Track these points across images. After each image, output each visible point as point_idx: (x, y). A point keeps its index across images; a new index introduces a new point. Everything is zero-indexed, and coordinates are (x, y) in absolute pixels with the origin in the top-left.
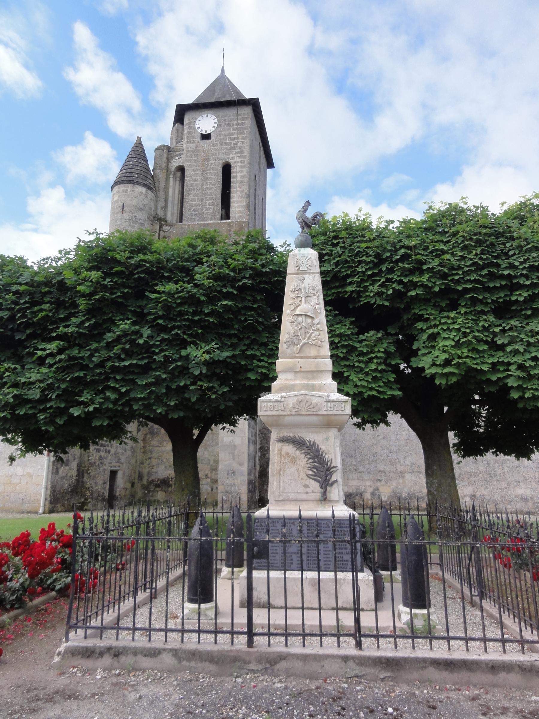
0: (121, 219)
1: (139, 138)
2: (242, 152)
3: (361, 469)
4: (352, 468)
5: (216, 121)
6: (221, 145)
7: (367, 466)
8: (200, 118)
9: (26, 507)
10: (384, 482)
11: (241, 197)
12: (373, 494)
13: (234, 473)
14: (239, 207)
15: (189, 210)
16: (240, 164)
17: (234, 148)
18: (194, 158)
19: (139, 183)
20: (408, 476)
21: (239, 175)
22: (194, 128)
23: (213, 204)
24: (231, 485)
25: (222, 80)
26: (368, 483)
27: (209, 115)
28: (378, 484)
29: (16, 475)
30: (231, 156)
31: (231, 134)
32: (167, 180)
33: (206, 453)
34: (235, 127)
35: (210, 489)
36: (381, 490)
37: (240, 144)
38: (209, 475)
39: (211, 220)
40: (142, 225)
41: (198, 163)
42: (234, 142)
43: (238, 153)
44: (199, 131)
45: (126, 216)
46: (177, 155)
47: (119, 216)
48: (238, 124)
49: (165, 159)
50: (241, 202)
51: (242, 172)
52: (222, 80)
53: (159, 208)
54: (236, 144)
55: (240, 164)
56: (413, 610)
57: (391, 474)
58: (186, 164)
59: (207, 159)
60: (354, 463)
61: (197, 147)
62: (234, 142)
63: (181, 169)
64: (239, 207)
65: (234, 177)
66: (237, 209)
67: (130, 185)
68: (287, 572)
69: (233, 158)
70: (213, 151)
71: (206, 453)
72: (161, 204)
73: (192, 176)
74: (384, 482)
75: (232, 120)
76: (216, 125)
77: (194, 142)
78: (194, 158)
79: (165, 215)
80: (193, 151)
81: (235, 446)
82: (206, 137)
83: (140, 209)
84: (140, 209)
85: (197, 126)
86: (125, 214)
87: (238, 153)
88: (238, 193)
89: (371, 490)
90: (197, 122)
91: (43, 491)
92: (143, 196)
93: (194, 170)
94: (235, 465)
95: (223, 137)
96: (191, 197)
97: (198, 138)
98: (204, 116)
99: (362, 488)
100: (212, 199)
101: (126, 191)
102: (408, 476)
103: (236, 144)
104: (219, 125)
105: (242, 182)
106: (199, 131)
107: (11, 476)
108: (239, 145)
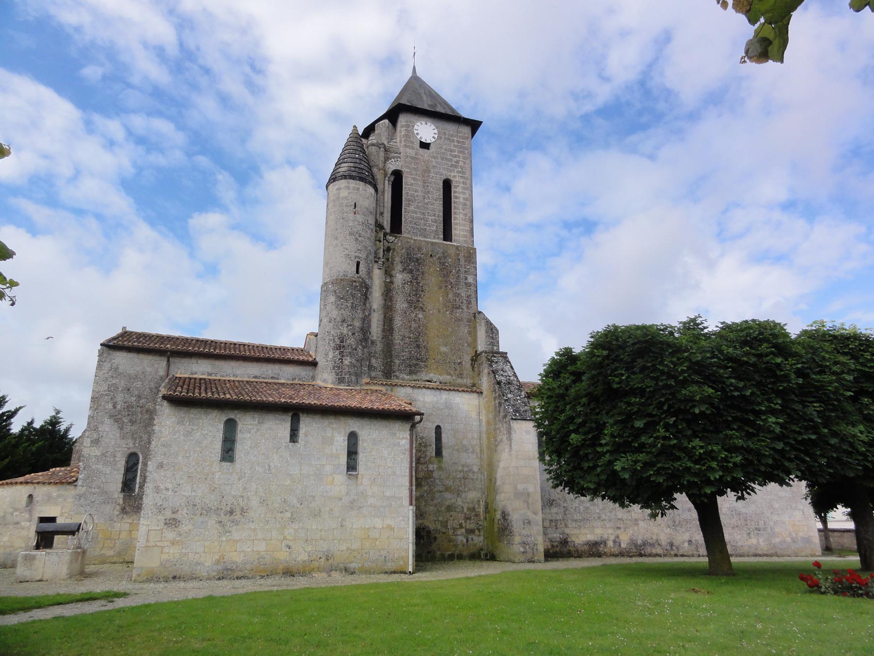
0: (354, 220)
2: (463, 173)
3: (603, 517)
4: (596, 516)
5: (436, 131)
6: (442, 159)
7: (608, 514)
8: (419, 124)
9: (390, 566)
10: (622, 530)
11: (465, 220)
12: (614, 542)
13: (529, 523)
14: (463, 231)
16: (461, 185)
17: (456, 167)
18: (413, 165)
20: (641, 523)
21: (461, 196)
22: (413, 133)
24: (527, 536)
25: (415, 83)
26: (610, 531)
27: (429, 124)
28: (618, 532)
29: (374, 528)
30: (453, 174)
31: (452, 151)
33: (459, 500)
34: (456, 143)
35: (465, 540)
36: (621, 537)
37: (461, 164)
38: (464, 525)
39: (434, 238)
41: (419, 173)
42: (455, 159)
43: (460, 172)
44: (419, 137)
45: (359, 217)
46: (394, 157)
47: (351, 216)
48: (459, 142)
49: (382, 159)
50: (464, 225)
51: (464, 193)
52: (415, 83)
54: (457, 162)
57: (628, 522)
59: (427, 171)
60: (597, 511)
61: (416, 154)
62: (455, 159)
64: (463, 231)
65: (456, 198)
67: (362, 183)
69: (454, 176)
70: (434, 164)
71: (459, 500)
74: (622, 530)
75: (452, 136)
76: (436, 136)
77: (413, 148)
78: (413, 165)
80: (413, 158)
81: (528, 494)
82: (425, 146)
85: (416, 132)
87: (460, 172)
88: (462, 216)
89: (612, 538)
90: (416, 127)
91: (411, 546)
93: (414, 179)
94: (530, 515)
95: (443, 151)
96: (412, 208)
97: (418, 145)
98: (423, 123)
99: (605, 536)
101: (358, 189)
102: (641, 523)
103: (457, 162)
104: (439, 137)
105: (465, 204)
106: (419, 137)
107: (369, 529)
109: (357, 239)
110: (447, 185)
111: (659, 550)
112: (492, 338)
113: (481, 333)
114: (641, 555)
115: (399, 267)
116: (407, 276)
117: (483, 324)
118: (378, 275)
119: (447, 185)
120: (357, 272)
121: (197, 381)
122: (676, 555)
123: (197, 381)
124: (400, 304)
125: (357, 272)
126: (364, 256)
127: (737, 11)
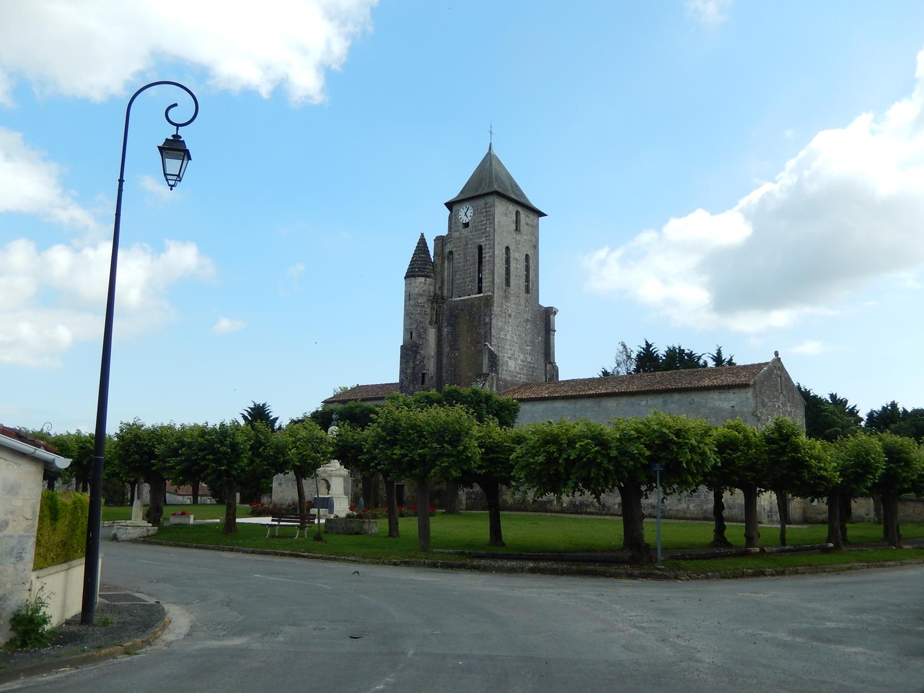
1: (422, 235)
17: (484, 233)
19: (419, 276)
32: (443, 263)
40: (423, 306)
63: (451, 253)
82: (466, 225)
83: (421, 295)
84: (421, 295)
93: (459, 254)
97: (461, 227)
104: (474, 214)
110: (480, 248)
114: (577, 513)
118: (432, 333)
122: (606, 514)
124: (446, 349)
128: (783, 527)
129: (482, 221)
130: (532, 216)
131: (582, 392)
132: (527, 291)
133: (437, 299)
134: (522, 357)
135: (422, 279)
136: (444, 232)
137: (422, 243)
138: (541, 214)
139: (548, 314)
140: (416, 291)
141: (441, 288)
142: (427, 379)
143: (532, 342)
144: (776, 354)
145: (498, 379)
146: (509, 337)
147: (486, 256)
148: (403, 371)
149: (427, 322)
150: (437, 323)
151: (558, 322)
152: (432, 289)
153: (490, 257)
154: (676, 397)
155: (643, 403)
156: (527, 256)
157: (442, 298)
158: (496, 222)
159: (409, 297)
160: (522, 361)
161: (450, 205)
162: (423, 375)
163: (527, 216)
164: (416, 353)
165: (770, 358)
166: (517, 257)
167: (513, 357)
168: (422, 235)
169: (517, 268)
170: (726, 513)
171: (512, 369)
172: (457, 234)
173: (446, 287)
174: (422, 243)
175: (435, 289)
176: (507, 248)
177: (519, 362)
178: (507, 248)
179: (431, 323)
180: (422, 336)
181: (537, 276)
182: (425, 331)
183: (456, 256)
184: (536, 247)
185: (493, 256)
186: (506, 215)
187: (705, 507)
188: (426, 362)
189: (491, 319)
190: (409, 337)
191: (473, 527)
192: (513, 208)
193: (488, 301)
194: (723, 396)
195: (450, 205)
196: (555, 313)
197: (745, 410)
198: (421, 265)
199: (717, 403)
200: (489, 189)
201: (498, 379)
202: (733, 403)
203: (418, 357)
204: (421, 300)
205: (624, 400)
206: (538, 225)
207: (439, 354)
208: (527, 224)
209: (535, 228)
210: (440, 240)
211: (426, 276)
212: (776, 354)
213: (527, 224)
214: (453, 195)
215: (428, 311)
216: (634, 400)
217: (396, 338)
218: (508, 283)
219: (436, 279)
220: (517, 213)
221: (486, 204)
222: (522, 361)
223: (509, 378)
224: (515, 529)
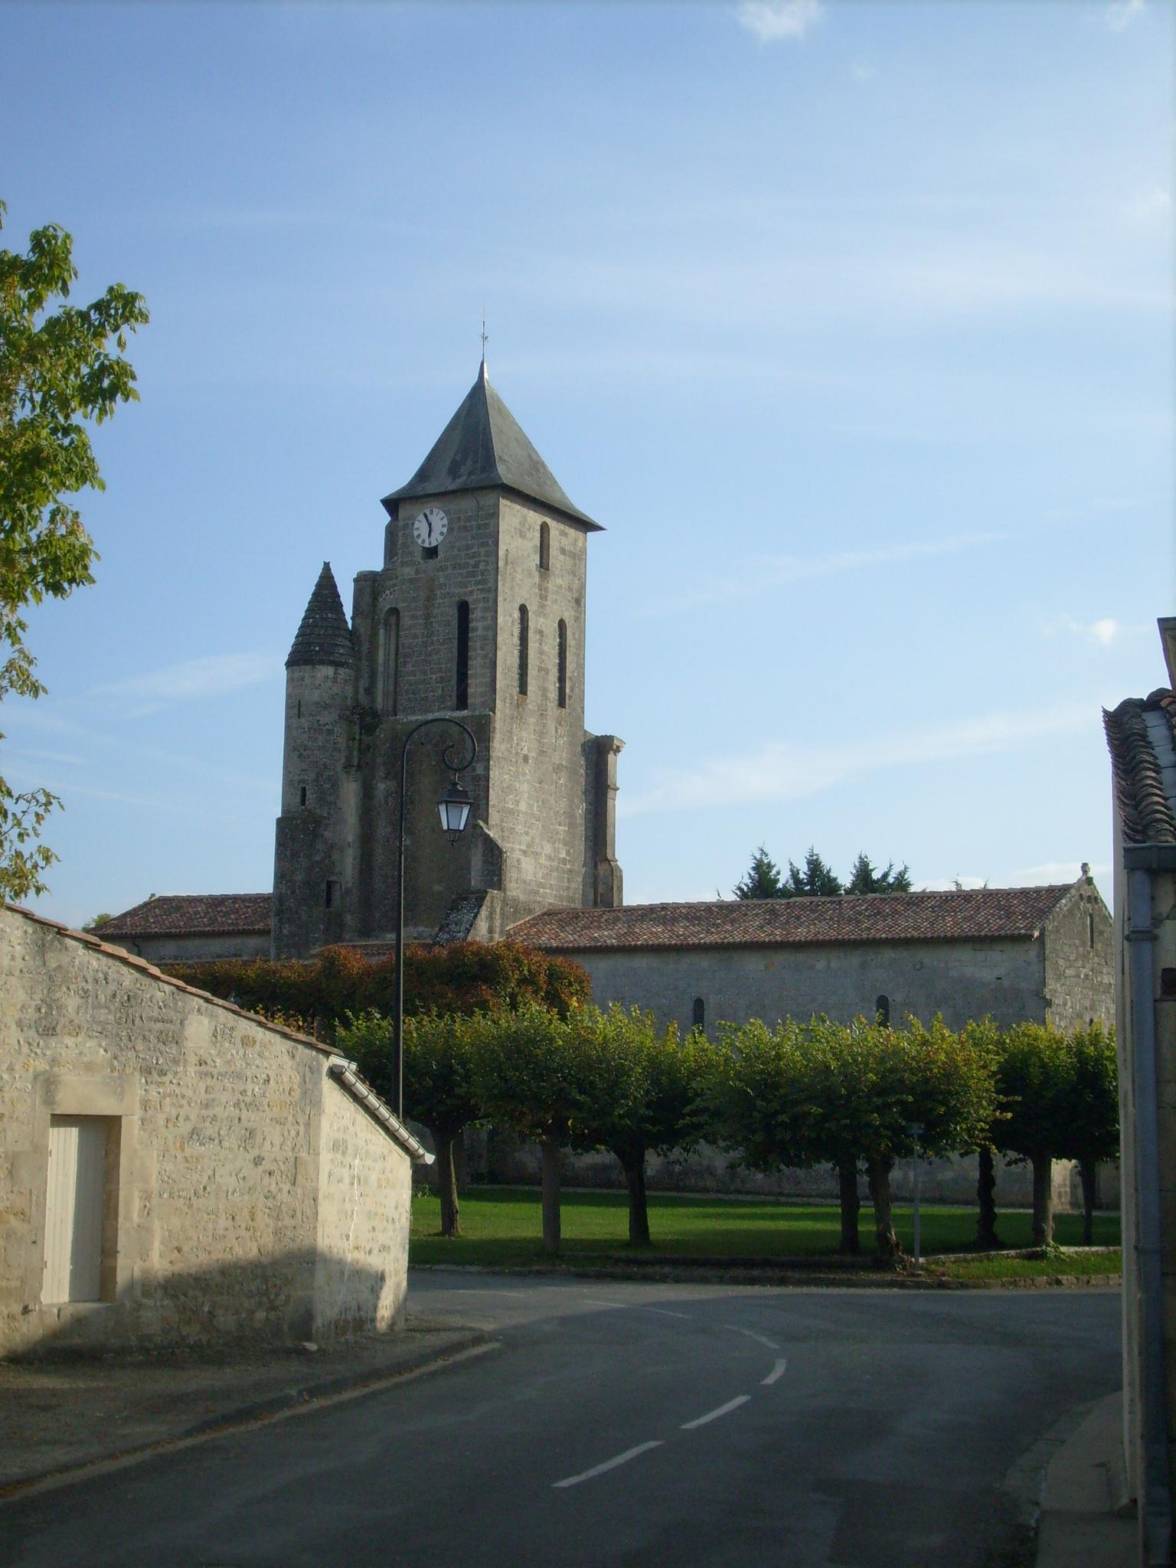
1: (327, 566)
15: (407, 692)
17: (472, 574)
19: (322, 662)
23: (441, 680)
32: (374, 634)
40: (330, 732)
42: (472, 562)
44: (420, 541)
53: (361, 691)
55: (481, 605)
56: (566, 1211)
58: (401, 606)
61: (417, 572)
62: (472, 562)
63: (395, 611)
66: (479, 690)
67: (308, 667)
68: (566, 1211)
69: (471, 592)
72: (363, 683)
73: (410, 627)
76: (445, 530)
79: (373, 700)
80: (411, 581)
82: (431, 553)
83: (326, 707)
84: (326, 707)
85: (416, 533)
86: (303, 720)
87: (478, 583)
92: (329, 683)
93: (413, 617)
97: (418, 556)
100: (440, 671)
101: (303, 679)
103: (476, 566)
104: (450, 530)
108: (482, 567)
109: (300, 756)
110: (464, 609)
111: (710, 1183)
112: (492, 864)
113: (477, 860)
114: (678, 1189)
115: (381, 772)
116: (392, 785)
117: (480, 845)
118: (350, 792)
119: (464, 609)
120: (303, 802)
121: (1112, 1214)
122: (738, 1192)
123: (1112, 1214)
124: (383, 829)
125: (303, 802)
126: (312, 776)
127: (356, 581)
128: (1089, 1212)
129: (468, 547)
130: (572, 532)
131: (687, 936)
132: (562, 703)
133: (363, 719)
134: (548, 849)
135: (329, 671)
136: (377, 564)
137: (326, 586)
138: (585, 525)
139: (598, 754)
140: (316, 696)
141: (370, 691)
142: (337, 895)
143: (571, 815)
144: (1085, 867)
145: (505, 902)
146: (523, 807)
147: (477, 624)
148: (280, 876)
149: (339, 768)
150: (362, 765)
151: (622, 769)
152: (349, 690)
153: (486, 628)
154: (889, 954)
155: (821, 965)
156: (562, 624)
157: (375, 714)
158: (501, 553)
159: (295, 708)
160: (549, 858)
161: (392, 504)
162: (330, 885)
163: (564, 534)
164: (315, 835)
165: (1073, 876)
166: (543, 624)
167: (535, 859)
168: (327, 566)
169: (543, 653)
170: (996, 1192)
171: (530, 877)
172: (408, 572)
173: (380, 685)
174: (326, 586)
175: (356, 692)
176: (523, 610)
177: (543, 861)
178: (523, 610)
179: (347, 767)
180: (328, 794)
181: (581, 666)
182: (335, 785)
183: (406, 621)
184: (579, 602)
185: (494, 627)
186: (523, 536)
187: (940, 1177)
188: (335, 856)
189: (487, 769)
190: (298, 799)
191: (609, 1223)
192: (535, 518)
193: (483, 730)
194: (980, 956)
195: (392, 504)
196: (618, 750)
197: (1023, 985)
198: (322, 636)
199: (969, 971)
200: (471, 468)
201: (505, 902)
202: (1000, 971)
203: (320, 846)
204: (328, 718)
205: (780, 958)
206: (584, 551)
207: (366, 838)
208: (563, 551)
209: (578, 557)
210: (366, 583)
211: (337, 664)
212: (1085, 867)
213: (563, 551)
214: (400, 478)
215: (342, 741)
216: (800, 957)
217: (268, 800)
218: (523, 689)
219: (358, 670)
220: (544, 529)
221: (479, 508)
222: (549, 858)
223: (522, 897)
224: (663, 1222)
